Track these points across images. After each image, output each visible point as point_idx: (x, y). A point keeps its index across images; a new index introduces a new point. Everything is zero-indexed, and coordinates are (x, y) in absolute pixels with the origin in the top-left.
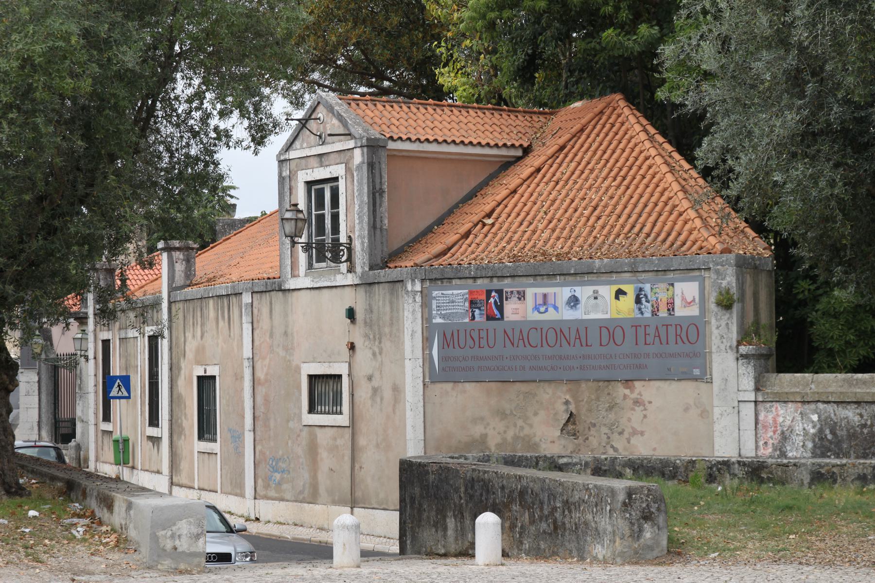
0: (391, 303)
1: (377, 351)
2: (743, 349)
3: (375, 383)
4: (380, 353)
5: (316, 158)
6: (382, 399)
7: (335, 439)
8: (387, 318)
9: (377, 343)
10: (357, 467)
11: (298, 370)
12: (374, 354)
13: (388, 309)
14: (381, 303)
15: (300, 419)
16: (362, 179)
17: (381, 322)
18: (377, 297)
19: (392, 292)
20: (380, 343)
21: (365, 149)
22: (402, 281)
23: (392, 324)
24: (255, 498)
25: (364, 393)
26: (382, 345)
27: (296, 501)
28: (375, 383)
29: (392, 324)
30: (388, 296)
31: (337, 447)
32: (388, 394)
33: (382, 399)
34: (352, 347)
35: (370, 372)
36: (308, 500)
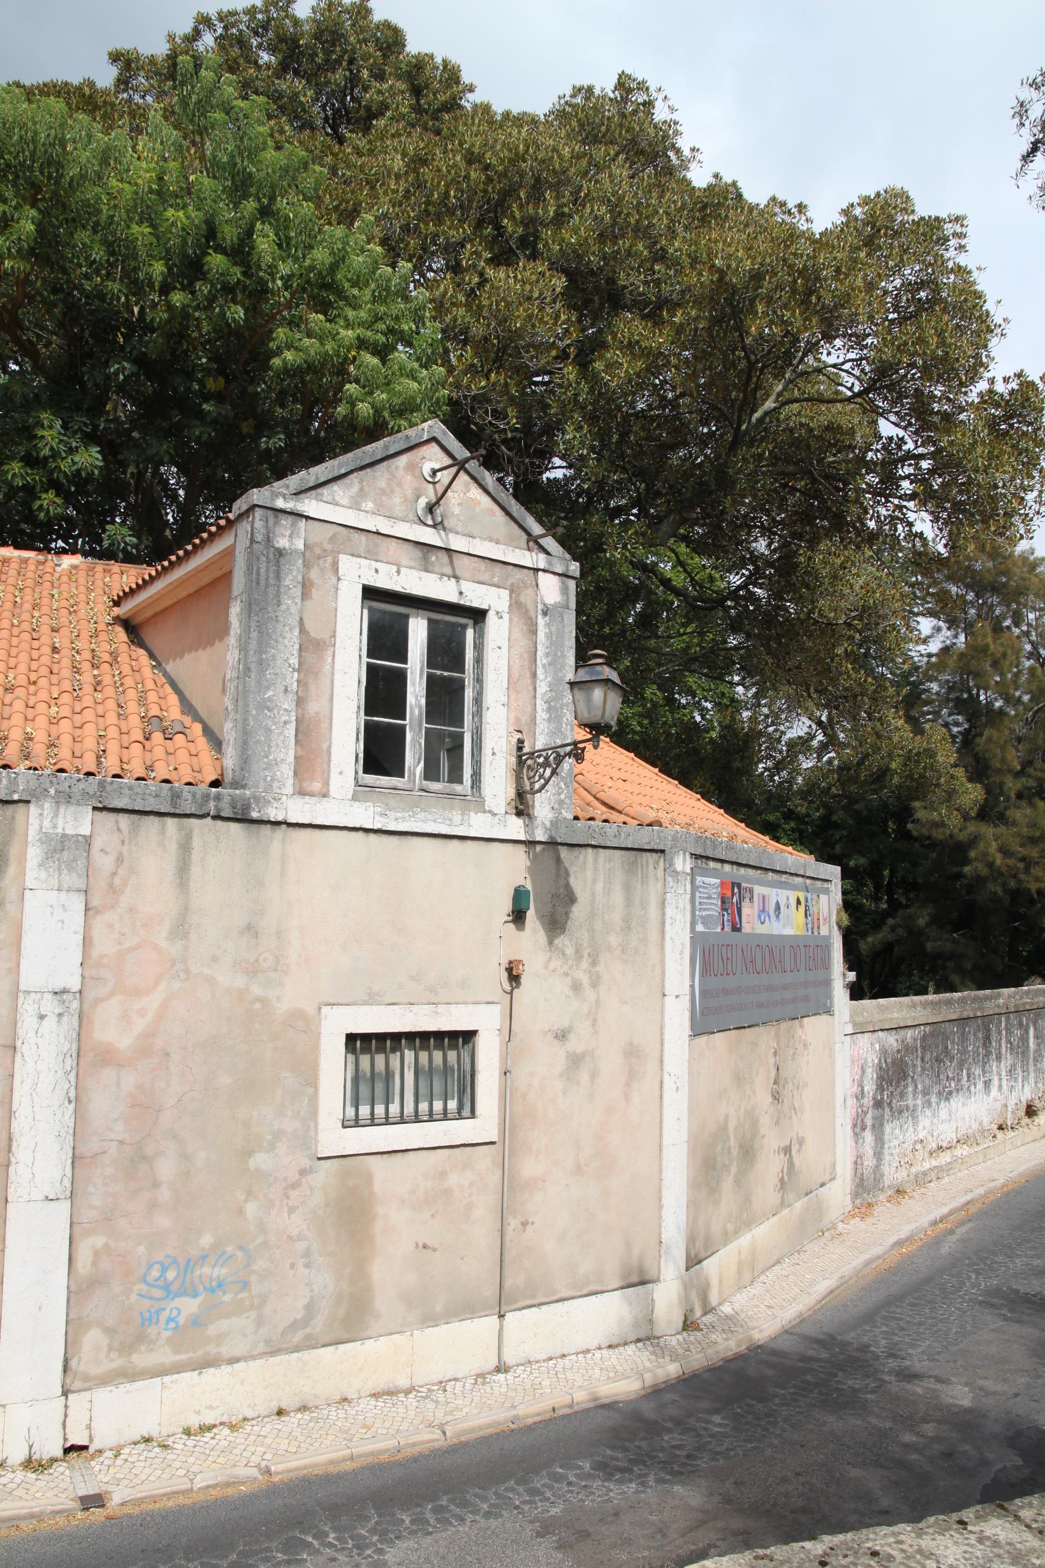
0: (627, 888)
1: (585, 980)
2: (641, 98)
3: (575, 1045)
4: (595, 984)
5: (522, 848)
6: (594, 1076)
7: (443, 1175)
8: (616, 917)
9: (585, 964)
10: (513, 1223)
11: (305, 1024)
12: (577, 987)
13: (618, 897)
14: (600, 886)
15: (306, 1137)
16: (560, 635)
17: (598, 926)
18: (589, 873)
19: (631, 869)
20: (594, 963)
21: (572, 584)
22: (663, 851)
23: (627, 928)
24: (65, 1393)
25: (543, 1064)
26: (600, 968)
27: (273, 1353)
28: (575, 1045)
29: (627, 928)
30: (619, 877)
31: (448, 1192)
32: (610, 1063)
33: (594, 1076)
34: (514, 977)
35: (565, 1023)
36: (328, 1338)
